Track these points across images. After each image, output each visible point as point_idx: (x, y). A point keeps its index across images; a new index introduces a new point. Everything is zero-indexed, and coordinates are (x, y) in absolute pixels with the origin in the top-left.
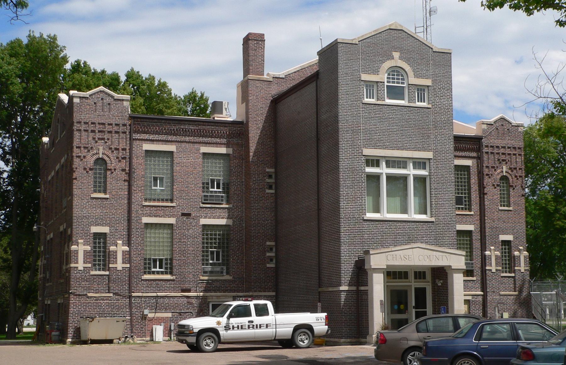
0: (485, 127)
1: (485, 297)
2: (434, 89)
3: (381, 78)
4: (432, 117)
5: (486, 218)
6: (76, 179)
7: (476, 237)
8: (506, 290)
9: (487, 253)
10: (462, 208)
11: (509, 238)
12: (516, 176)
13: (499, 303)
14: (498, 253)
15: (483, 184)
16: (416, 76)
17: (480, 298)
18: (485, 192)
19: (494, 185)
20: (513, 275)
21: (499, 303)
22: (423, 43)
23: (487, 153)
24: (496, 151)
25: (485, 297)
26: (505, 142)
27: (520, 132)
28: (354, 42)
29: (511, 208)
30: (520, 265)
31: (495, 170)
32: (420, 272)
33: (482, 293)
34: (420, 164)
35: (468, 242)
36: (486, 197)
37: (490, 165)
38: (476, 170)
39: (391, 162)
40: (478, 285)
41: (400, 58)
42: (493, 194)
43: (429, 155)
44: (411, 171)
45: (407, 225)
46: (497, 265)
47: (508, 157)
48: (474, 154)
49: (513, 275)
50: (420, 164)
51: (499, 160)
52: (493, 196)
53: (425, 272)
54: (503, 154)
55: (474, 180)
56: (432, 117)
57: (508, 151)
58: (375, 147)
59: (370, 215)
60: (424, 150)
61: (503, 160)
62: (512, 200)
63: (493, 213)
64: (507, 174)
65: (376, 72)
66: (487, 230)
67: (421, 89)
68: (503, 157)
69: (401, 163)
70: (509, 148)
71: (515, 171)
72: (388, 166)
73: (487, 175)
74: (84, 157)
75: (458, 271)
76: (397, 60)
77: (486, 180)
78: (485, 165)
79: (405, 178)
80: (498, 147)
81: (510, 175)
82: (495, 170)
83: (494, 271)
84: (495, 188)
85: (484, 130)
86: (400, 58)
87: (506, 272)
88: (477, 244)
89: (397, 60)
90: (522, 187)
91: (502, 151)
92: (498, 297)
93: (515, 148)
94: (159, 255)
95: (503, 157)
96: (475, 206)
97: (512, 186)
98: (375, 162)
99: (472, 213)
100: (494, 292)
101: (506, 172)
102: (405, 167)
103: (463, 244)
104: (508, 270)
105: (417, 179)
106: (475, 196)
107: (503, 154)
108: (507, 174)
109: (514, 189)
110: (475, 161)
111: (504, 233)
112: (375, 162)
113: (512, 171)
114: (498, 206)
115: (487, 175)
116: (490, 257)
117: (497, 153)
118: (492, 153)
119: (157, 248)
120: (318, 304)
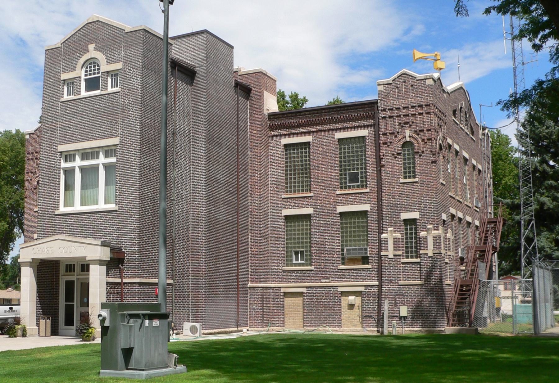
0: (381, 88)
1: (380, 287)
2: (125, 72)
3: (77, 74)
4: (120, 101)
5: (383, 194)
6: (26, 198)
7: (373, 217)
8: (408, 278)
9: (384, 236)
10: (358, 186)
11: (415, 215)
12: (423, 140)
13: (397, 295)
14: (399, 235)
15: (380, 156)
16: (109, 62)
17: (375, 290)
18: (383, 163)
19: (393, 154)
20: (418, 260)
21: (397, 295)
22: (117, 27)
23: (384, 118)
24: (396, 113)
25: (380, 287)
26: (408, 101)
27: (428, 86)
28: (57, 46)
29: (417, 180)
30: (426, 248)
31: (396, 136)
32: (71, 265)
33: (377, 283)
34: (109, 151)
35: (365, 225)
36: (383, 169)
37: (388, 132)
38: (373, 140)
39: (86, 154)
40: (374, 273)
41: (95, 49)
42: (393, 165)
43: (115, 141)
44: (102, 160)
45: (92, 217)
46: (395, 249)
47: (412, 119)
48: (371, 122)
49: (418, 260)
50: (109, 151)
51: (400, 124)
52: (392, 168)
53: (74, 265)
54: (405, 116)
55: (370, 152)
56: (120, 101)
57: (411, 111)
58: (69, 142)
59: (63, 209)
60: (112, 136)
61: (405, 123)
62: (418, 169)
63: (393, 188)
64: (411, 139)
65: (73, 69)
66: (384, 209)
67: (114, 74)
68: (405, 119)
69: (86, 154)
70: (413, 107)
71: (422, 134)
72: (83, 159)
73: (385, 143)
74: (31, 180)
75: (95, 262)
76: (92, 52)
77: (383, 150)
78: (381, 133)
79: (95, 168)
80: (398, 109)
81: (416, 139)
82: (396, 136)
83: (391, 256)
84: (396, 157)
85: (380, 93)
86: (95, 49)
87: (412, 257)
88: (373, 226)
89: (92, 52)
90: (431, 151)
91: (404, 112)
92: (396, 288)
93: (421, 106)
94: (299, 247)
95: (405, 119)
96: (372, 183)
97: (418, 153)
98: (69, 157)
99: (368, 190)
100: (391, 282)
101: (410, 137)
102: (98, 157)
103: (359, 227)
104: (414, 254)
105: (107, 167)
106: (371, 170)
107: (405, 116)
108: (411, 139)
109: (420, 155)
110: (371, 129)
111: (407, 211)
112: (69, 157)
113: (418, 135)
114: (399, 178)
115: (385, 143)
116: (386, 240)
117: (397, 116)
118: (390, 117)
119: (409, 236)
120: (500, 287)
